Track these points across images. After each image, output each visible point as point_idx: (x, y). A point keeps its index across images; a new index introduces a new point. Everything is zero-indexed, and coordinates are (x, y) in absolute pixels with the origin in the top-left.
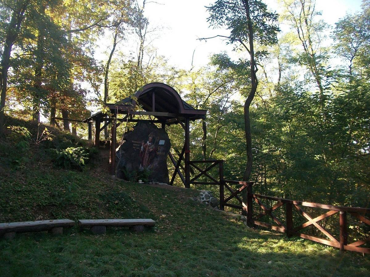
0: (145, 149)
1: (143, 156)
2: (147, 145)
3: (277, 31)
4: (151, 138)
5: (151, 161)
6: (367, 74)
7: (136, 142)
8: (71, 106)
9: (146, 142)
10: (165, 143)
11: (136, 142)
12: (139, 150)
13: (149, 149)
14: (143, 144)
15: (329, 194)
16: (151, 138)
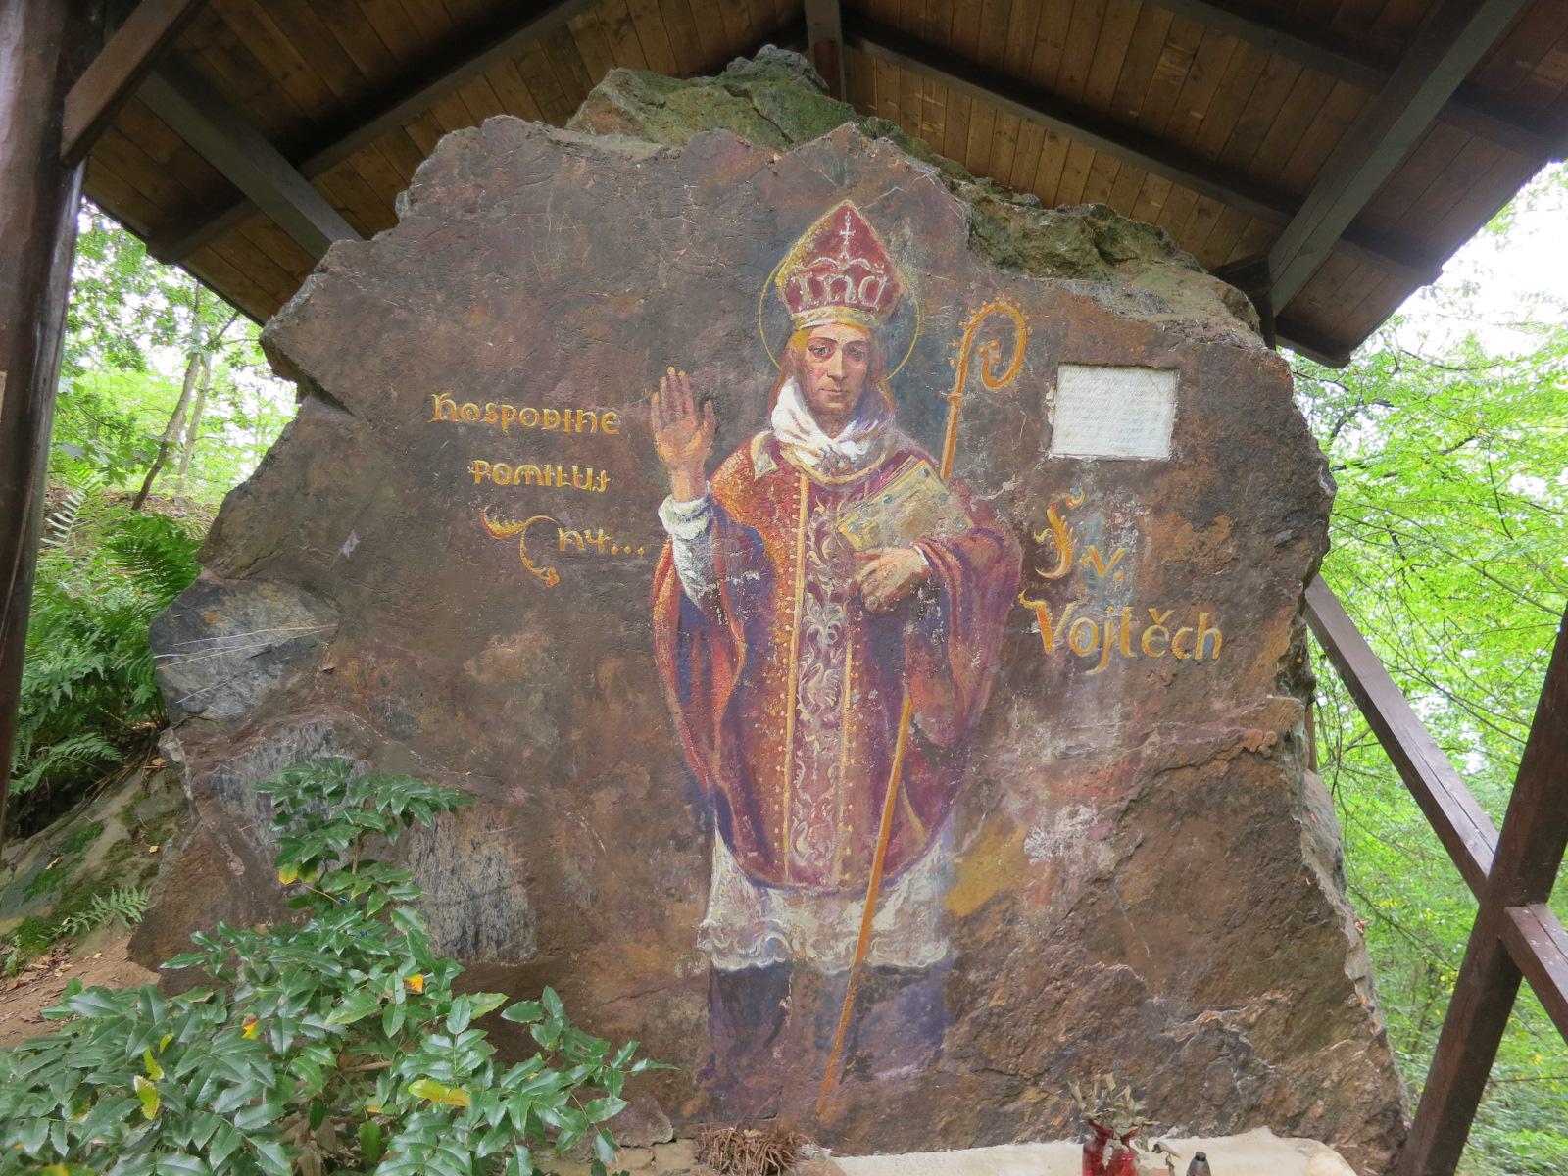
0: (745, 543)
1: (725, 684)
3: (752, 470)
4: (831, 322)
5: (935, 780)
6: (578, 429)
7: (526, 416)
9: (732, 419)
10: (1179, 430)
11: (526, 416)
12: (622, 582)
13: (846, 559)
14: (678, 443)
16: (831, 322)
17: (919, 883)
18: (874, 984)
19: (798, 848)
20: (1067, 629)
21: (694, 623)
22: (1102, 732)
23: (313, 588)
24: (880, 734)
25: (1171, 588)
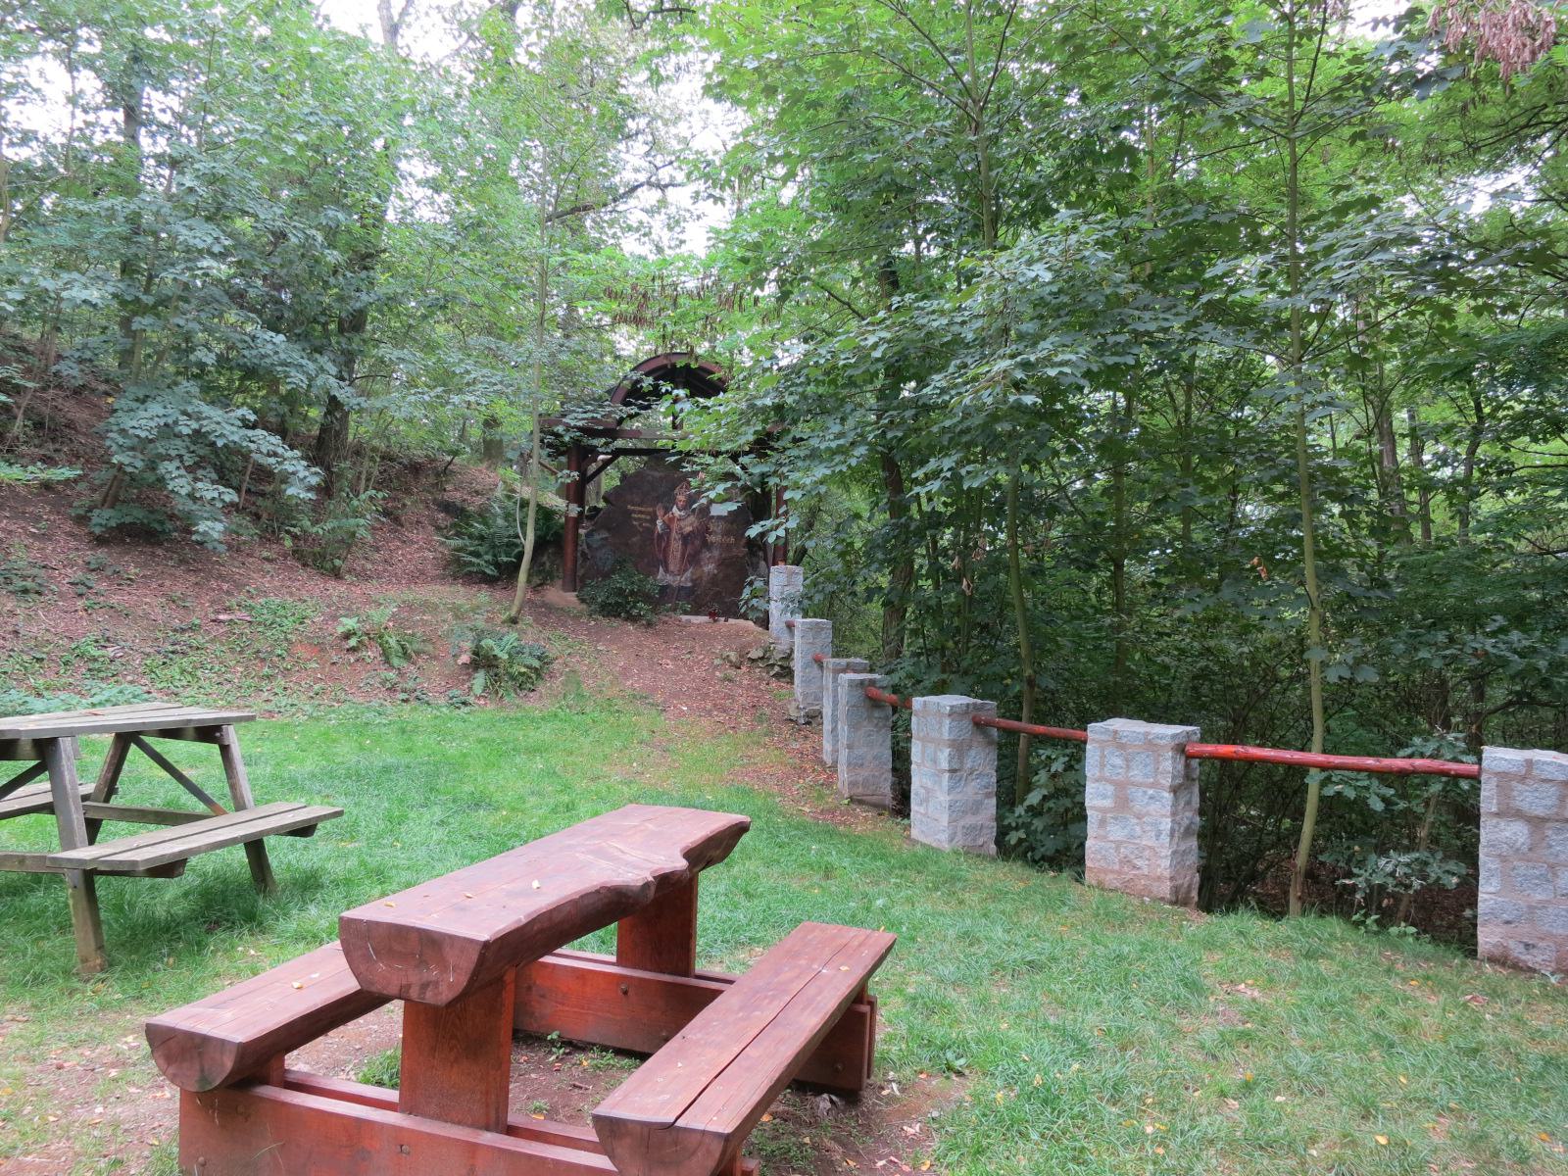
0: (667, 526)
5: (692, 559)
9: (667, 510)
12: (651, 531)
14: (660, 512)
17: (688, 574)
18: (681, 588)
19: (672, 568)
20: (712, 539)
21: (660, 536)
22: (716, 553)
23: (609, 530)
24: (470, 573)
25: (727, 533)
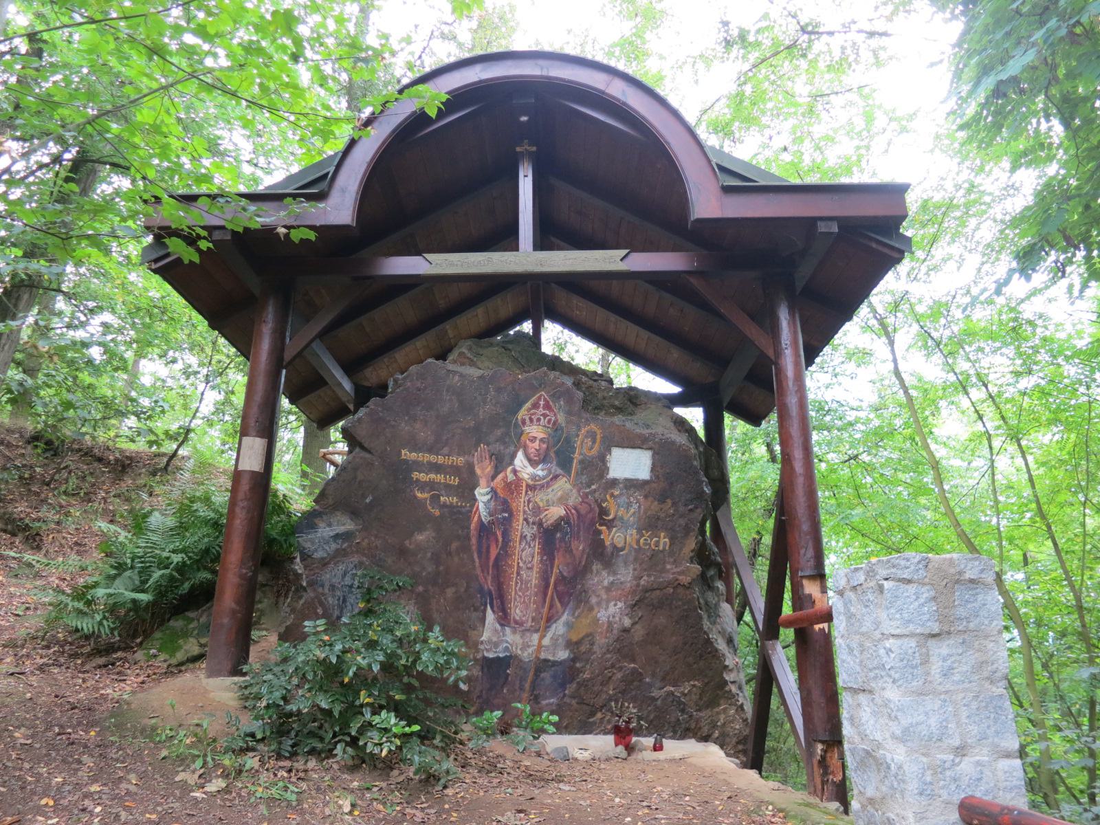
0: (503, 503)
1: (494, 552)
2: (519, 480)
8: (177, 177)
9: (501, 462)
12: (460, 516)
14: (483, 469)
15: (12, 9)
